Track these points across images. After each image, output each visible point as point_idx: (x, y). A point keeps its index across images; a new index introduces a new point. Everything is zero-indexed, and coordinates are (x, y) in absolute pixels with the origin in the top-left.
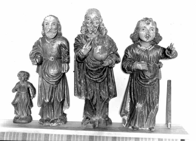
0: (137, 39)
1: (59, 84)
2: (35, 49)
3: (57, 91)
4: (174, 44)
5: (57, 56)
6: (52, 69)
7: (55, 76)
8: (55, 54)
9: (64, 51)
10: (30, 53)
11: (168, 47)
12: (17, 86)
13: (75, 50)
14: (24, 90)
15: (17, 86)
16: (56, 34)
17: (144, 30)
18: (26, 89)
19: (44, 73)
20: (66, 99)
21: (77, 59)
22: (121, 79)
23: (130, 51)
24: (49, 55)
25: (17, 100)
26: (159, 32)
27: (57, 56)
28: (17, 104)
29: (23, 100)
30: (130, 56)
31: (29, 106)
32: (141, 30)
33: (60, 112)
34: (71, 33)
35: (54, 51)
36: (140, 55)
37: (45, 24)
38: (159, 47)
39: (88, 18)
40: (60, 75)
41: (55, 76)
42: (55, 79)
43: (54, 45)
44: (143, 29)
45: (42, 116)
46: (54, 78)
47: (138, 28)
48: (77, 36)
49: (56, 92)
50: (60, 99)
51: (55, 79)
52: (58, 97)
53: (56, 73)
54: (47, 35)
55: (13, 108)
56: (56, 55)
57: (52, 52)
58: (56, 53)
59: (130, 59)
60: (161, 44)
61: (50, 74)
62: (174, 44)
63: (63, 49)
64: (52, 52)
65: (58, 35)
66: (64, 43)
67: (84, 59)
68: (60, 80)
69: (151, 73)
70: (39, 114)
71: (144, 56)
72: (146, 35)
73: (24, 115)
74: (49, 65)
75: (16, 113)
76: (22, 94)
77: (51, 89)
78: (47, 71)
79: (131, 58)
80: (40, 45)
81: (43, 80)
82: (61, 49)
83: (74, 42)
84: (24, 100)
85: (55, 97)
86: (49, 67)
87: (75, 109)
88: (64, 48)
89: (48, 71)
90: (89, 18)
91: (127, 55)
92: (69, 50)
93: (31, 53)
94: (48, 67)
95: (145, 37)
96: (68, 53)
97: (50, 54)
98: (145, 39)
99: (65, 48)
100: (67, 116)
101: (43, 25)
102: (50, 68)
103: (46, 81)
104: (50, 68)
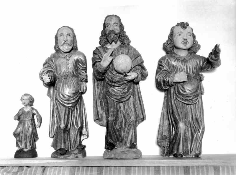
0: (170, 47)
1: (76, 107)
2: (47, 66)
3: (74, 116)
4: (216, 52)
5: (74, 73)
6: (68, 88)
7: (72, 96)
8: (71, 70)
9: (82, 67)
10: (40, 72)
11: (73, 64)
12: (20, 112)
13: (94, 65)
14: (27, 118)
15: (20, 112)
16: (71, 47)
17: (181, 35)
18: (30, 115)
19: (57, 94)
20: (84, 125)
21: (96, 74)
22: (152, 99)
23: (165, 61)
24: (63, 72)
25: (19, 129)
26: (196, 40)
27: (74, 73)
28: (19, 134)
29: (26, 129)
30: (166, 68)
31: (34, 137)
32: (176, 36)
33: (78, 141)
34: (88, 44)
35: (69, 67)
36: (176, 66)
37: (58, 36)
38: (198, 56)
39: (107, 25)
40: (77, 95)
41: (72, 96)
42: (72, 100)
43: (69, 60)
44: (180, 35)
45: (55, 148)
46: (71, 99)
47: (171, 36)
48: (95, 49)
49: (73, 117)
50: (77, 126)
51: (72, 100)
52: (76, 123)
53: (74, 93)
54: (61, 48)
55: (14, 140)
56: (72, 72)
57: (68, 68)
58: (72, 69)
59: (166, 71)
60: (200, 53)
61: (66, 94)
62: (216, 52)
63: (80, 65)
64: (68, 68)
65: (74, 49)
66: (82, 58)
67: (104, 74)
68: (77, 101)
69: (192, 86)
70: (52, 146)
71: (181, 67)
72: (184, 41)
73: (27, 148)
74: (64, 83)
75: (17, 145)
76: (25, 122)
77: (67, 113)
78: (61, 90)
79: (166, 70)
80: (53, 62)
81: (57, 102)
82: (78, 64)
83: (91, 56)
84: (27, 128)
85: (72, 122)
86: (64, 86)
87: (95, 140)
88: (81, 63)
89: (62, 90)
90: (108, 25)
91: (161, 66)
92: (86, 66)
93: (42, 71)
94: (63, 85)
95: (182, 44)
96: (86, 69)
97: (65, 70)
98: (181, 46)
99: (83, 64)
100: (86, 149)
101: (56, 38)
102: (65, 87)
103: (60, 103)
104: (65, 87)
